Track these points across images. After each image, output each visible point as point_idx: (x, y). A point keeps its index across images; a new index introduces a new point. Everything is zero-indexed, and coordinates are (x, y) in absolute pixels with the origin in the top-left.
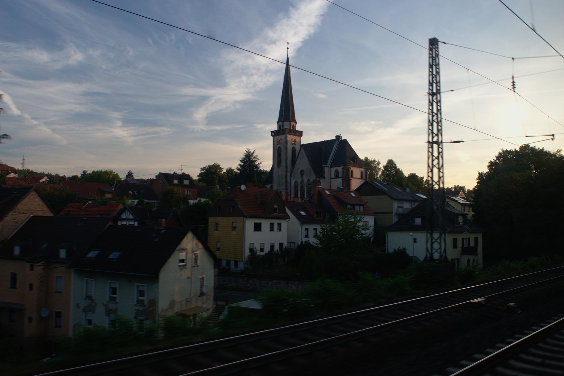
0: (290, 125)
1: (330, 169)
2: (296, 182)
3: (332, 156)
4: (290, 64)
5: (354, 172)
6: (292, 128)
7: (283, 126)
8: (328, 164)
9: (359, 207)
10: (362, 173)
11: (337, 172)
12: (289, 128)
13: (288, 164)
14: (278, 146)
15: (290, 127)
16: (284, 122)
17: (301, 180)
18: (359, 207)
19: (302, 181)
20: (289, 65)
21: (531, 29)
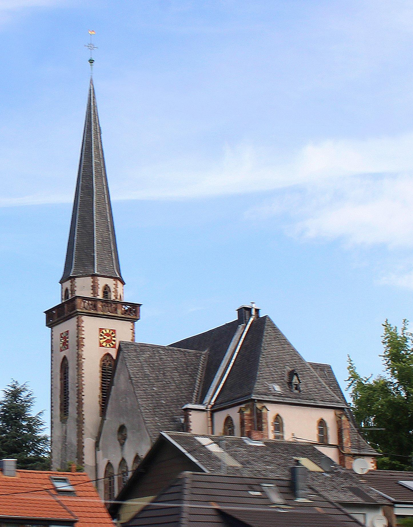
0: (94, 288)
1: (212, 417)
2: (109, 465)
3: (233, 348)
4: (204, 444)
5: (285, 422)
6: (100, 296)
7: (73, 291)
8: (204, 403)
9: (133, 340)
10: (322, 423)
11: (228, 420)
12: (91, 296)
13: (84, 408)
14: (63, 354)
15: (95, 292)
16: (74, 278)
17: (119, 459)
18: (133, 340)
19: (123, 460)
20: (204, 446)
21: (55, 518)
